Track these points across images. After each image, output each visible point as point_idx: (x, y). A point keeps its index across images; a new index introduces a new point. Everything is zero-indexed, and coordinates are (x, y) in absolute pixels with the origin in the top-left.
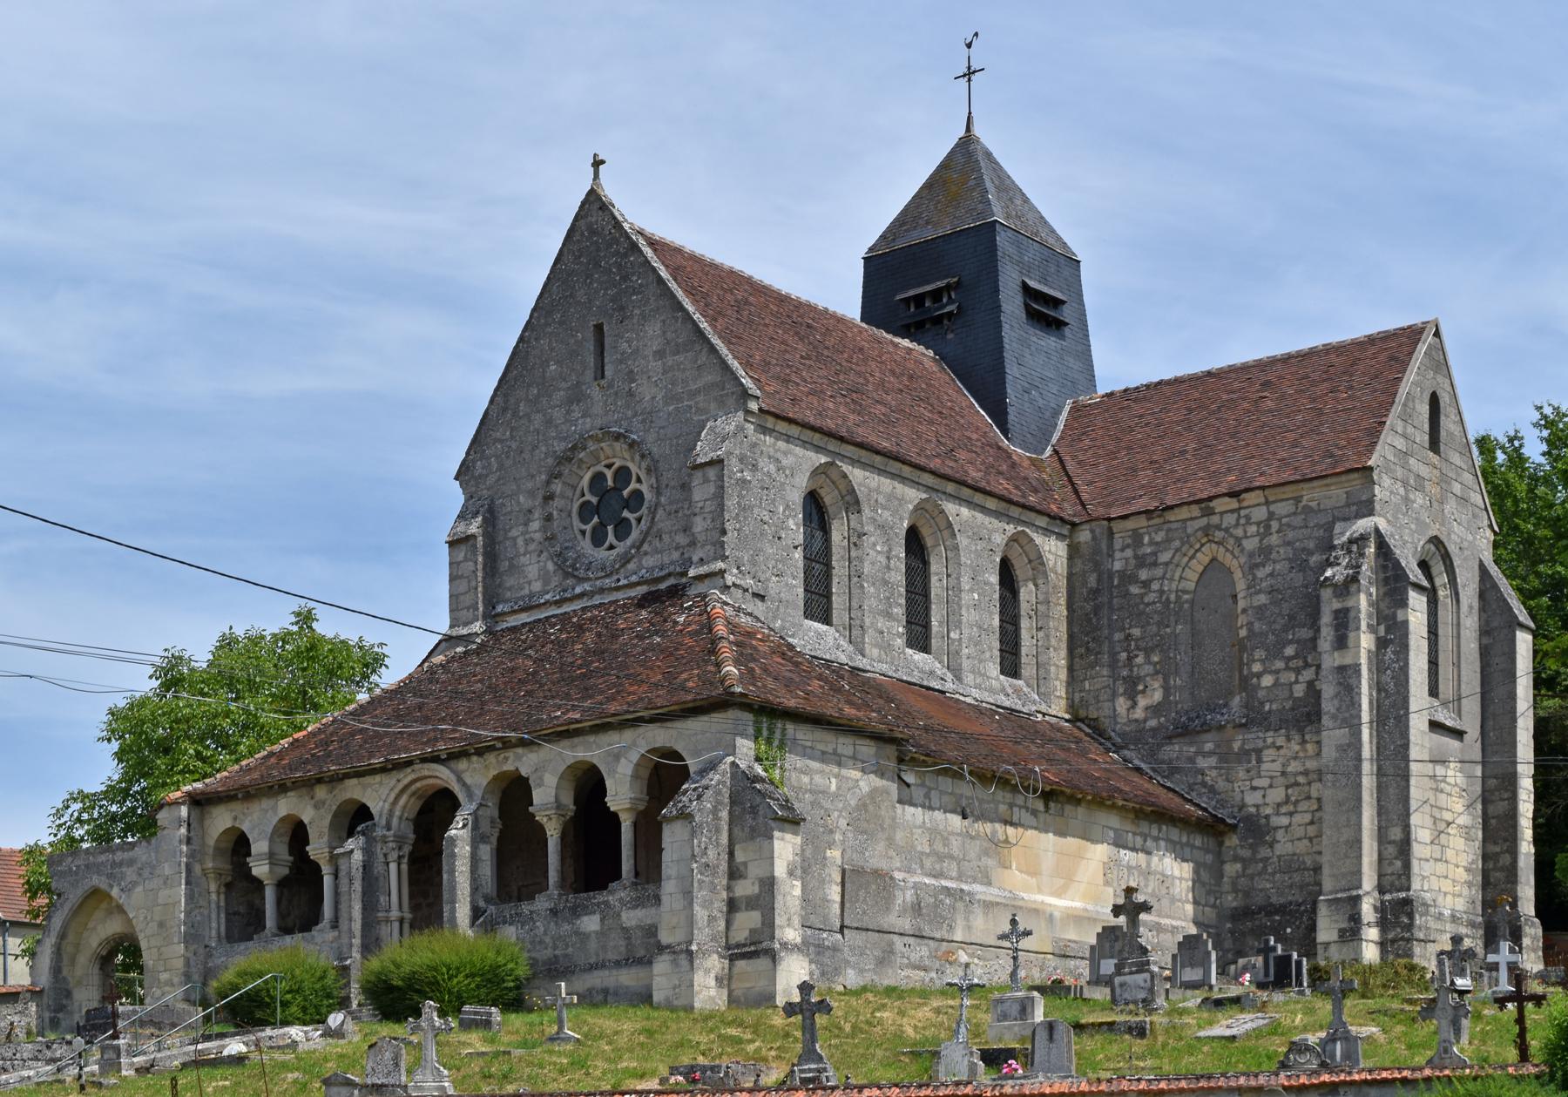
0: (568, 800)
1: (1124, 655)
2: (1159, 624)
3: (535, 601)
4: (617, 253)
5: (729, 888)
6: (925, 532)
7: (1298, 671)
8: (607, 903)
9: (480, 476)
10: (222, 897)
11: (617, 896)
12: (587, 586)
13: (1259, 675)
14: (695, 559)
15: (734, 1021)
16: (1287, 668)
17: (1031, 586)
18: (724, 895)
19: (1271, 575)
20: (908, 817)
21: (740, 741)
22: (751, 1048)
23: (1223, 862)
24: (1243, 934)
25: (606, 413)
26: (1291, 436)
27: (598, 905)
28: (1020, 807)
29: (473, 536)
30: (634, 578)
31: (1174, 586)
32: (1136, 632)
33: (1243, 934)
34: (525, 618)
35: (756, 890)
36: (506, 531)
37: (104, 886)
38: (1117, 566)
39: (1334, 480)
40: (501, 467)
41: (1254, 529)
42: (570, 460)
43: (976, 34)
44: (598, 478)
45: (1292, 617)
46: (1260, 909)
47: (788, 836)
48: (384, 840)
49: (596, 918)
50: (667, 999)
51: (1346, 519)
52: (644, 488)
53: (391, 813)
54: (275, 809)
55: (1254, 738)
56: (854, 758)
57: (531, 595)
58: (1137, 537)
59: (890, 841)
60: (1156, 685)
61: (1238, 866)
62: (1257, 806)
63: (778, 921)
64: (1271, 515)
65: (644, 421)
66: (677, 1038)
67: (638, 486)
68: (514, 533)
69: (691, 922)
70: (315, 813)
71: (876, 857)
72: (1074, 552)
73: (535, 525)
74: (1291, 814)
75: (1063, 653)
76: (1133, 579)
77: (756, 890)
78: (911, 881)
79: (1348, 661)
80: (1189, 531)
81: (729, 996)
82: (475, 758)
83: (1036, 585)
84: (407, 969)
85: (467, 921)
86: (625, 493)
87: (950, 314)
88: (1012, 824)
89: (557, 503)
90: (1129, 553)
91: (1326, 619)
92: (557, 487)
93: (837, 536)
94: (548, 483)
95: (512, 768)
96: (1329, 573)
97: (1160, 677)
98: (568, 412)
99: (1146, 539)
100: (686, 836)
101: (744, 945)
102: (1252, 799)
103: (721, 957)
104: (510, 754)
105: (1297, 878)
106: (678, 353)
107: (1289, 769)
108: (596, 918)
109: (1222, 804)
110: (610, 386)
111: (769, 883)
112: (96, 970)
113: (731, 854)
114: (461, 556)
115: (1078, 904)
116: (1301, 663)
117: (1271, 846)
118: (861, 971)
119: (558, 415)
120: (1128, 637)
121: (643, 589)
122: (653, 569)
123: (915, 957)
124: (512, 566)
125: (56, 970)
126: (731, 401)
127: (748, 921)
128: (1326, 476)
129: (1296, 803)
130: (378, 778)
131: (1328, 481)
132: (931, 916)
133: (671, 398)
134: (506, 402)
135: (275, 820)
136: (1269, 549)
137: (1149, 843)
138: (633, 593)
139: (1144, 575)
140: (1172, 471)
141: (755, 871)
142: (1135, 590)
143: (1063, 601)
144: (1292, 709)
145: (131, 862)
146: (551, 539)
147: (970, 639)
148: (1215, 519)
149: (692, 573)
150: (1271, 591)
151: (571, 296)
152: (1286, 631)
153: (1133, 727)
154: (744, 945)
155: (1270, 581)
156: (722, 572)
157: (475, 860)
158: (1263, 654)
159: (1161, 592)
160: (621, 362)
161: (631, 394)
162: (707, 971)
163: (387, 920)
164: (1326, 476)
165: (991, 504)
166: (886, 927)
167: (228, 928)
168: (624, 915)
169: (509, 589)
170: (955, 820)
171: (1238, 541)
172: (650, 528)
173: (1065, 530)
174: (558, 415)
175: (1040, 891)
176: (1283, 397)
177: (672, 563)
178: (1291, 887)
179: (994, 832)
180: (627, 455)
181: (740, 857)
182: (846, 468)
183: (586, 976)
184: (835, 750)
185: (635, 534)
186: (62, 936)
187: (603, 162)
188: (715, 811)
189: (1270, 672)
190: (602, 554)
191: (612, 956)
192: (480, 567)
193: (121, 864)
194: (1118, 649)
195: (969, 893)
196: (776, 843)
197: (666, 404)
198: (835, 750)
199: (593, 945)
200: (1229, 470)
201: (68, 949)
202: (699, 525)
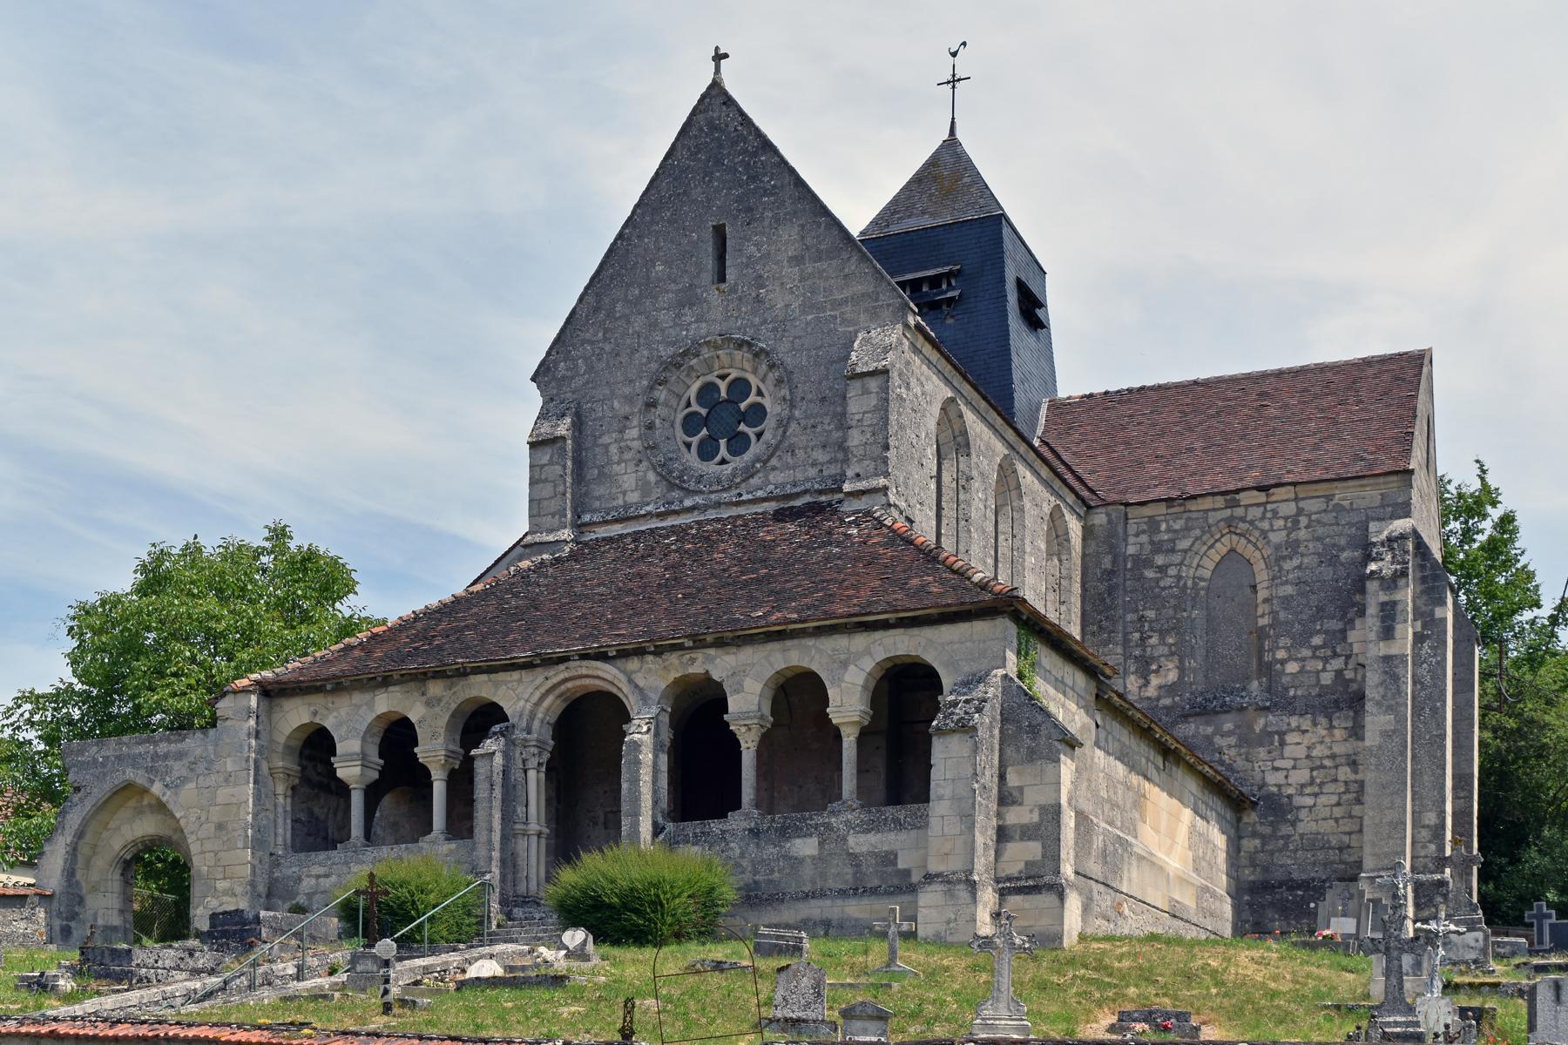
1: (1137, 635)
2: (1175, 608)
3: (632, 512)
4: (745, 151)
5: (999, 815)
7: (1326, 660)
8: (828, 826)
9: (563, 377)
11: (842, 818)
12: (699, 500)
13: (1283, 662)
14: (850, 473)
16: (1314, 657)
18: (994, 822)
19: (1299, 567)
23: (1240, 838)
24: (1263, 907)
25: (727, 319)
26: (1311, 440)
27: (816, 827)
29: (563, 438)
30: (760, 494)
32: (1151, 614)
33: (1263, 907)
34: (617, 530)
35: (1035, 818)
38: (1131, 550)
39: (1371, 481)
40: (590, 369)
41: (1281, 523)
42: (678, 366)
43: (964, 44)
44: (708, 390)
45: (1320, 609)
46: (1281, 884)
51: (1379, 519)
52: (767, 402)
53: (532, 716)
58: (1153, 524)
60: (1171, 666)
61: (1257, 842)
62: (1279, 786)
64: (1300, 511)
65: (775, 329)
67: (759, 399)
68: (606, 439)
72: (1088, 532)
73: (634, 433)
74: (1316, 795)
76: (1148, 563)
77: (1035, 818)
79: (1394, 651)
82: (650, 658)
85: (649, 837)
86: (743, 406)
87: (950, 301)
89: (661, 410)
90: (1144, 538)
91: (1372, 610)
94: (651, 388)
95: (702, 671)
96: (1373, 567)
98: (678, 316)
99: (1163, 527)
100: (966, 752)
101: (1018, 879)
102: (1273, 779)
104: (699, 655)
105: (1321, 856)
106: (820, 260)
107: (1314, 753)
109: (1243, 781)
110: (733, 290)
111: (1052, 813)
112: (117, 876)
113: (1002, 777)
114: (545, 459)
116: (1329, 653)
117: (1293, 824)
119: (665, 318)
120: (1141, 618)
121: (771, 506)
122: (783, 485)
124: (601, 474)
125: (70, 873)
126: (886, 313)
127: (1021, 854)
128: (1363, 477)
129: (1322, 784)
130: (516, 675)
133: (807, 307)
134: (598, 302)
135: (371, 717)
136: (1297, 542)
138: (759, 508)
139: (1160, 560)
140: (1184, 465)
142: (1150, 574)
143: (1078, 579)
144: (1319, 695)
148: (1239, 512)
149: (847, 487)
150: (1299, 583)
152: (1314, 622)
154: (1018, 879)
155: (1297, 573)
156: (886, 488)
160: (747, 266)
161: (758, 300)
162: (985, 905)
163: (525, 834)
164: (1363, 477)
167: (293, 840)
168: (851, 840)
170: (1120, 769)
171: (1264, 534)
174: (665, 318)
176: (1286, 406)
177: (807, 480)
178: (1314, 864)
180: (747, 366)
181: (1013, 780)
182: (963, 408)
183: (801, 905)
185: (755, 449)
186: (80, 835)
187: (726, 56)
188: (991, 728)
189: (1296, 660)
190: (711, 468)
192: (569, 471)
193: (166, 757)
194: (1130, 629)
197: (804, 312)
199: (807, 872)
200: (1250, 467)
201: (84, 849)
202: (855, 439)
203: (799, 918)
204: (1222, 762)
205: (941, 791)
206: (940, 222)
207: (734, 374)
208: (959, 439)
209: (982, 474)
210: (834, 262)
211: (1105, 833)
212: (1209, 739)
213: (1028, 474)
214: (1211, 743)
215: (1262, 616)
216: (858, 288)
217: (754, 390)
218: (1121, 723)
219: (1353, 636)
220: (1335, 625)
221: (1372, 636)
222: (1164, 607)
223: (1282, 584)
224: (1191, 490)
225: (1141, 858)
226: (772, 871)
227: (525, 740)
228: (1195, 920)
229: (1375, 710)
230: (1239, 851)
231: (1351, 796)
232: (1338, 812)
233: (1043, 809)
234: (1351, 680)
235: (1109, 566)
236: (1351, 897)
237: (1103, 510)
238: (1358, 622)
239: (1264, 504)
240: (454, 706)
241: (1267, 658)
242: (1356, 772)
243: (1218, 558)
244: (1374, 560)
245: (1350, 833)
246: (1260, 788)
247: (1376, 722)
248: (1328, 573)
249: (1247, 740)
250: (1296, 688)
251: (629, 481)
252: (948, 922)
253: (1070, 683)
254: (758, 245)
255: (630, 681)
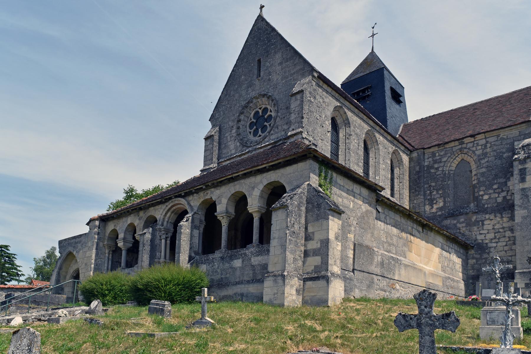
0: (232, 210)
1: (429, 192)
2: (442, 181)
5: (305, 246)
6: (368, 143)
8: (245, 254)
10: (111, 255)
12: (250, 149)
13: (482, 196)
15: (308, 315)
16: (494, 192)
17: (398, 169)
18: (303, 249)
19: (487, 162)
20: (379, 226)
21: (312, 175)
22: (322, 336)
23: (468, 259)
26: (492, 119)
28: (415, 229)
29: (213, 135)
31: (447, 169)
35: (319, 245)
36: (224, 135)
37: (72, 251)
38: (426, 164)
39: (515, 127)
40: (224, 114)
41: (480, 147)
42: (246, 107)
47: (336, 220)
48: (160, 230)
49: (240, 261)
50: (270, 300)
51: (519, 140)
54: (127, 221)
55: (480, 217)
56: (360, 195)
57: (231, 155)
58: (434, 154)
59: (372, 233)
60: (441, 201)
61: (474, 261)
62: (482, 240)
63: (330, 262)
64: (487, 142)
65: (274, 88)
66: (274, 325)
68: (227, 135)
69: (285, 260)
70: (136, 220)
71: (367, 240)
72: (411, 160)
73: (234, 131)
74: (497, 242)
75: (408, 191)
76: (432, 167)
77: (319, 245)
78: (380, 253)
80: (454, 150)
81: (303, 299)
82: (195, 195)
83: (400, 169)
84: (145, 280)
86: (266, 116)
88: (413, 235)
89: (242, 123)
90: (431, 159)
91: (516, 172)
92: (242, 117)
93: (341, 135)
96: (516, 156)
97: (442, 198)
99: (437, 154)
102: (479, 237)
103: (299, 279)
104: (209, 192)
107: (496, 227)
108: (240, 261)
109: (468, 239)
110: (262, 79)
111: (326, 243)
113: (306, 228)
115: (432, 269)
116: (500, 190)
117: (488, 253)
118: (361, 290)
119: (243, 93)
120: (430, 186)
121: (271, 146)
123: (381, 285)
124: (225, 146)
127: (314, 261)
129: (499, 238)
130: (160, 206)
131: (512, 128)
132: (389, 266)
136: (486, 153)
137: (450, 250)
139: (436, 166)
140: (445, 134)
141: (318, 236)
142: (433, 171)
143: (408, 175)
144: (497, 206)
145: (80, 242)
146: (239, 135)
147: (382, 180)
148: (464, 146)
151: (250, 52)
152: (494, 180)
153: (432, 215)
155: (487, 164)
156: (301, 132)
157: (192, 236)
158: (484, 188)
159: (443, 171)
161: (269, 80)
162: (292, 286)
165: (389, 137)
166: (371, 271)
168: (252, 259)
169: (224, 154)
170: (395, 231)
171: (474, 152)
172: (274, 125)
173: (408, 153)
174: (243, 93)
175: (421, 263)
179: (407, 237)
181: (310, 229)
182: (346, 110)
183: (234, 287)
184: (353, 189)
185: (268, 129)
186: (60, 269)
187: (263, 6)
188: (299, 206)
189: (487, 194)
190: (257, 138)
191: (246, 278)
195: (400, 260)
196: (330, 222)
197: (282, 80)
198: (353, 189)
199: (238, 273)
203: (234, 292)
204: (460, 233)
205: (275, 235)
206: (365, 73)
207: (264, 106)
208: (346, 122)
209: (356, 134)
210: (291, 61)
211: (382, 255)
212: (455, 225)
213: (381, 138)
214: (456, 226)
215: (474, 180)
216: (298, 68)
217: (269, 110)
218: (394, 212)
219: (509, 184)
220: (502, 180)
221: (517, 181)
222: (438, 181)
223: (481, 168)
224: (446, 141)
225: (406, 266)
226: (227, 273)
227: (160, 229)
228: (442, 290)
229: (519, 209)
230: (467, 264)
231: (511, 242)
232: (506, 248)
233: (322, 241)
234: (509, 200)
235: (418, 170)
236: (492, 280)
237: (416, 152)
238: (511, 178)
239: (473, 142)
240: (145, 219)
241: (476, 195)
242: (513, 233)
243: (457, 163)
244: (516, 154)
245: (511, 256)
246: (475, 241)
247: (519, 213)
248: (499, 162)
249: (469, 224)
250: (488, 204)
251: (232, 147)
252: (274, 295)
253: (358, 192)
254: (269, 62)
255: (189, 203)
